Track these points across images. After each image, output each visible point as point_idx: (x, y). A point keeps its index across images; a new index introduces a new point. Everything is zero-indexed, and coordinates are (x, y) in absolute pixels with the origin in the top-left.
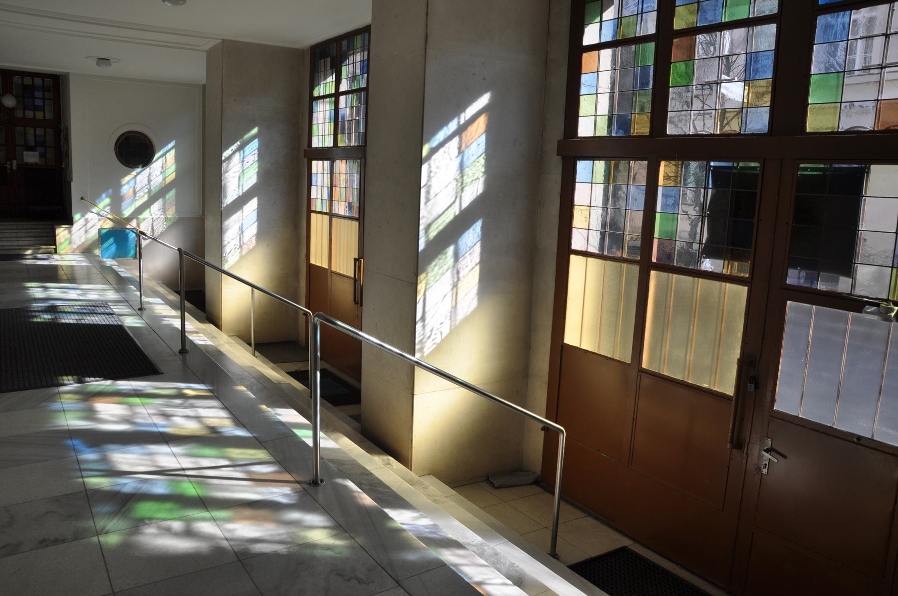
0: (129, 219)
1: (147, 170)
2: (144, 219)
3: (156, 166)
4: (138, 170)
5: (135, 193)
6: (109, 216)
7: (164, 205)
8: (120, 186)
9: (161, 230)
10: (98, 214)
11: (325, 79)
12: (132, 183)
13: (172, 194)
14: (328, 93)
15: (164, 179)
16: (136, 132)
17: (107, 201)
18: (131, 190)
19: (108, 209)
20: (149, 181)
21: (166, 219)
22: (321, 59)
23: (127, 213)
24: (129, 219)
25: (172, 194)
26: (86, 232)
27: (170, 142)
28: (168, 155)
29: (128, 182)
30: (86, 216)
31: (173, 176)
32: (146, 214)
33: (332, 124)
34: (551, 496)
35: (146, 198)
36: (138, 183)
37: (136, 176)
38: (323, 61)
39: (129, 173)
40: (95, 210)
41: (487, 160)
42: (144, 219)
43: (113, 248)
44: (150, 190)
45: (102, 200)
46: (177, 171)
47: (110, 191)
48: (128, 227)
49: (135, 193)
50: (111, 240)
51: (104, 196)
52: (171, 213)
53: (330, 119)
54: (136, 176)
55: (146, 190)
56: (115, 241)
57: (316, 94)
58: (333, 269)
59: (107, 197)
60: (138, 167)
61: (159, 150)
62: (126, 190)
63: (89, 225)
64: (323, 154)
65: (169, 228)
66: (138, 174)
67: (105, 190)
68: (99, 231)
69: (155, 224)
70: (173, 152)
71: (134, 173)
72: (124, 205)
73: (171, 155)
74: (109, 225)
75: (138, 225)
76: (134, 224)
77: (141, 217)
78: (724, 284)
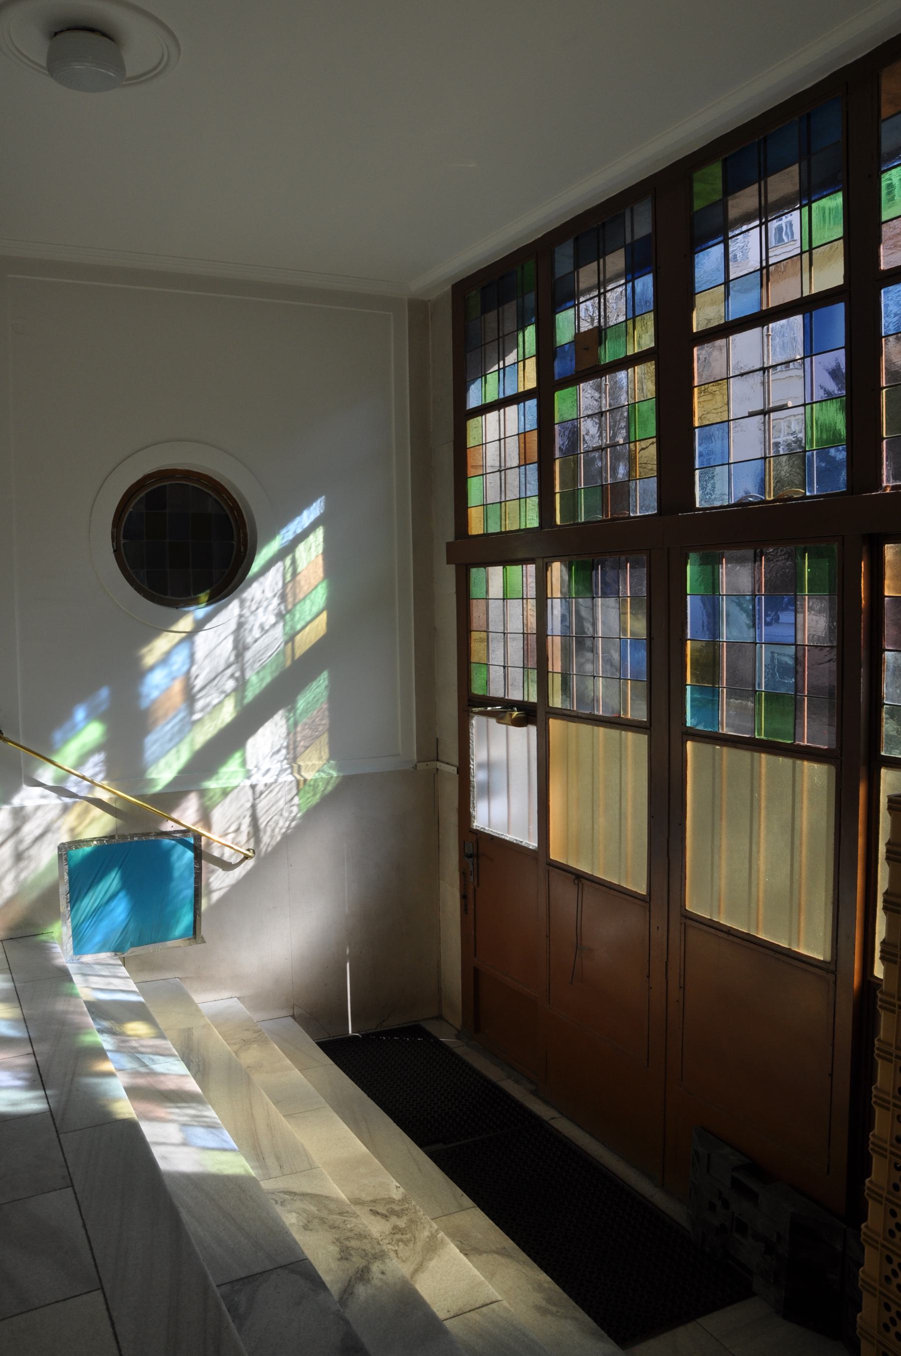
0: (171, 798)
1: (232, 610)
2: (225, 793)
3: (262, 590)
4: (200, 612)
5: (190, 696)
6: (105, 796)
7: (291, 732)
8: (136, 673)
9: (283, 825)
10: (60, 790)
11: (502, 356)
12: (179, 660)
13: (315, 694)
14: (509, 392)
15: (291, 639)
16: (188, 474)
17: (92, 732)
18: (178, 686)
19: (93, 767)
20: (240, 648)
21: (300, 785)
22: (485, 310)
23: (163, 773)
24: (171, 798)
25: (315, 694)
26: (19, 857)
27: (307, 504)
28: (301, 549)
29: (165, 660)
30: (17, 801)
31: (320, 626)
32: (230, 773)
33: (533, 471)
34: (325, 1038)
35: (228, 713)
36: (201, 656)
37: (190, 636)
38: (492, 316)
39: (163, 627)
40: (47, 774)
41: (324, 559)
42: (225, 793)
43: (120, 910)
44: (242, 684)
45: (74, 731)
46: (333, 607)
47: (104, 693)
48: (169, 826)
49: (190, 696)
50: (112, 881)
51: (80, 714)
52: (318, 767)
53: (524, 462)
54: (190, 636)
55: (230, 684)
56: (127, 884)
57: (474, 400)
58: (555, 854)
59: (91, 716)
60: (195, 602)
61: (271, 536)
62: (158, 684)
63: (31, 830)
64: (503, 549)
65: (311, 815)
66: (199, 626)
67: (81, 692)
68: (64, 850)
69: (262, 805)
70: (317, 539)
71: (185, 624)
72: (153, 743)
73: (311, 553)
74: (98, 826)
75: (205, 817)
76: (187, 814)
77: (212, 784)
78: (596, 728)
